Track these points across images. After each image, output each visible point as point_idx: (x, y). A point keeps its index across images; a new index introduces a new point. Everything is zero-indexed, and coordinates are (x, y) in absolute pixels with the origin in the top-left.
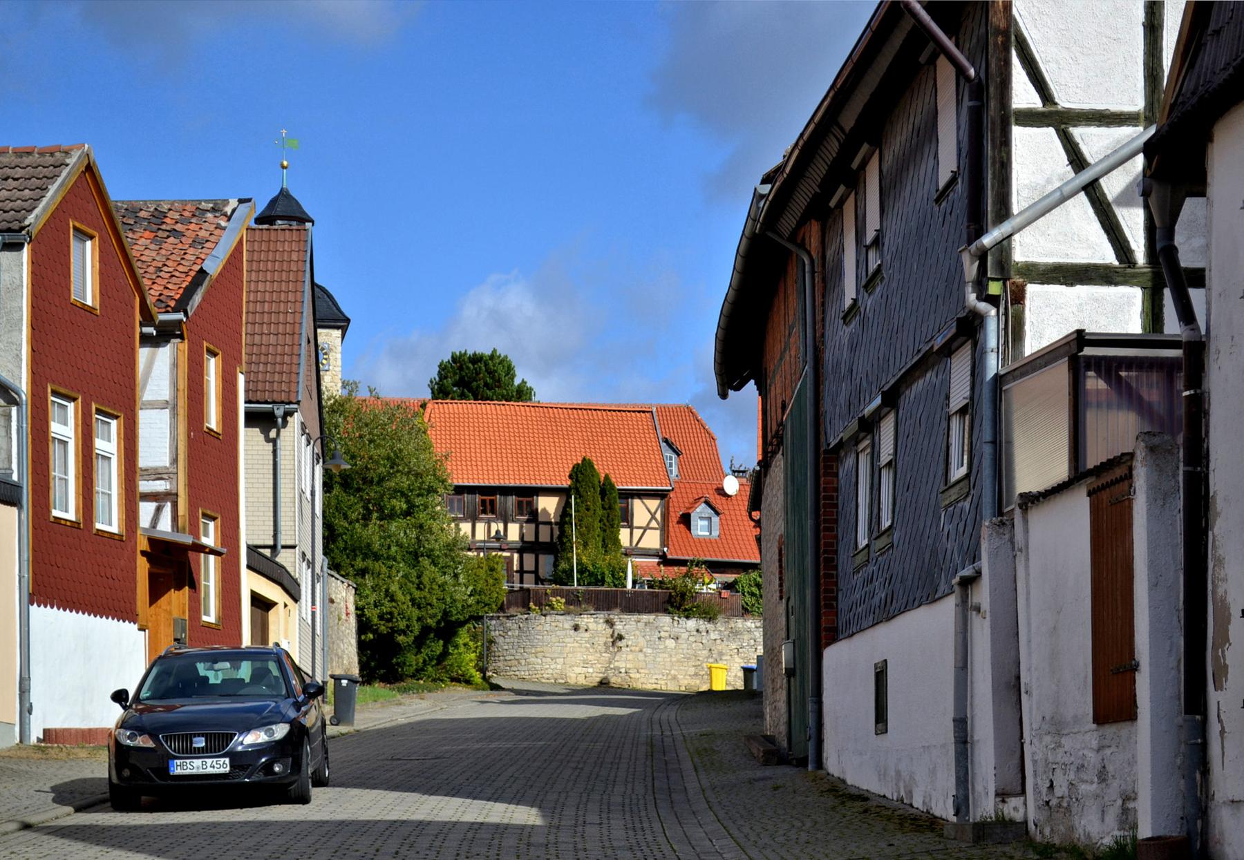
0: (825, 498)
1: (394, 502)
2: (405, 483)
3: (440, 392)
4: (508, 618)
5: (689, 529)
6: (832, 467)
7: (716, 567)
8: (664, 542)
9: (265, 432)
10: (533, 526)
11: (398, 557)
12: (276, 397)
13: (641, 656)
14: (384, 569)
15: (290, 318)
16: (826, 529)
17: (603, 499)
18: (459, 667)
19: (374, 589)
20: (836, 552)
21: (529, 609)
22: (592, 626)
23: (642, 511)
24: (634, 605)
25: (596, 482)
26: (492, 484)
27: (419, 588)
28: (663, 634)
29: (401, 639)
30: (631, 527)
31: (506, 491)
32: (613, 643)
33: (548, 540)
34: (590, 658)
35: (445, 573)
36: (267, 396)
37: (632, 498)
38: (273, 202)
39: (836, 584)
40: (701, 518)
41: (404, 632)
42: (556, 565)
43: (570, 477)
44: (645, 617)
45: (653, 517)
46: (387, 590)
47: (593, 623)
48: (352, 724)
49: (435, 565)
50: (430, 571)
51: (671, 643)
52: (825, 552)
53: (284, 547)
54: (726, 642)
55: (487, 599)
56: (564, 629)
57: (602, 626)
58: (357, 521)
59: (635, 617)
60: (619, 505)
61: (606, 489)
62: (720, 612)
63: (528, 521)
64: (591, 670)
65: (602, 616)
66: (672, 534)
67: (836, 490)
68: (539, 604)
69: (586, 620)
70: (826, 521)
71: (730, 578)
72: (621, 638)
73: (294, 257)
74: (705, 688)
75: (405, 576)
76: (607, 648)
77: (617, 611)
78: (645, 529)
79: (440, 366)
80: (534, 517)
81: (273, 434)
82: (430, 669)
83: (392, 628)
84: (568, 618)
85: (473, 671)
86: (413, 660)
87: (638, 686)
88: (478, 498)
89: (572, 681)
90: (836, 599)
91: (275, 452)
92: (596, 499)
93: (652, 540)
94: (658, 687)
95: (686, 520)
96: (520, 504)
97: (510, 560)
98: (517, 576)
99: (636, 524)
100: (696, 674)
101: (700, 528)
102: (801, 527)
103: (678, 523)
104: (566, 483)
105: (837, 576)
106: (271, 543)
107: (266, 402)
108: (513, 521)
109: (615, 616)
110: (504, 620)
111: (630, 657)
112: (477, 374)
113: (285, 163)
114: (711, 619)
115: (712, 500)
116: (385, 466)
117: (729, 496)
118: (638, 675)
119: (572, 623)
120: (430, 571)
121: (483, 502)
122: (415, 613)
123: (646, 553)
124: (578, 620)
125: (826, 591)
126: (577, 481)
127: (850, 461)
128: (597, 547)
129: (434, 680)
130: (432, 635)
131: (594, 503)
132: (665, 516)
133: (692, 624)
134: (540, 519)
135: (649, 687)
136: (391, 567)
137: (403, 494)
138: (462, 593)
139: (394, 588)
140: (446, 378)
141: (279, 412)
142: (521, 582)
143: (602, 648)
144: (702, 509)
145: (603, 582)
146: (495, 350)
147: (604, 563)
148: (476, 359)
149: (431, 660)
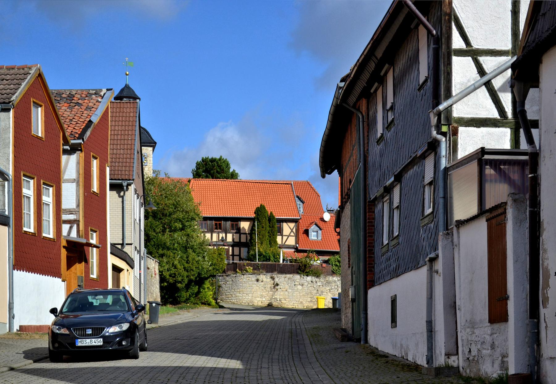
0: (369, 222)
1: (176, 224)
2: (181, 216)
3: (197, 175)
4: (227, 276)
5: (308, 236)
6: (372, 209)
7: (320, 253)
8: (297, 242)
9: (119, 193)
10: (238, 235)
11: (178, 249)
12: (123, 177)
13: (286, 293)
14: (172, 254)
15: (129, 142)
16: (369, 236)
17: (269, 223)
18: (205, 298)
19: (167, 263)
20: (374, 247)
21: (237, 272)
22: (265, 280)
23: (287, 228)
24: (283, 270)
25: (266, 215)
26: (220, 216)
27: (187, 263)
28: (296, 283)
29: (179, 285)
30: (282, 235)
31: (226, 219)
32: (274, 287)
33: (245, 241)
34: (264, 294)
35: (199, 256)
36: (119, 177)
37: (283, 222)
38: (122, 90)
39: (374, 261)
40: (313, 231)
41: (180, 282)
42: (248, 252)
43: (255, 213)
44: (288, 276)
45: (292, 231)
46: (173, 264)
47: (265, 278)
48: (157, 323)
49: (195, 252)
50: (192, 255)
51: (300, 287)
52: (369, 246)
53: (127, 244)
54: (324, 287)
55: (217, 268)
56: (252, 281)
57: (269, 280)
58: (160, 232)
59: (284, 275)
60: (277, 225)
61: (271, 218)
62: (322, 273)
63: (236, 233)
64: (264, 299)
65: (269, 275)
66: (300, 238)
67: (374, 219)
68: (241, 270)
69: (262, 277)
70: (369, 233)
71: (326, 258)
72: (277, 285)
73: (132, 115)
74: (315, 307)
75: (181, 257)
76: (271, 289)
77: (276, 273)
78: (288, 236)
79: (197, 163)
80: (238, 231)
81: (122, 194)
82: (192, 299)
83: (175, 280)
84: (254, 276)
85: (211, 300)
86: (185, 295)
87: (285, 306)
88: (214, 222)
89: (256, 304)
90: (374, 267)
91: (123, 202)
92: (266, 223)
93: (291, 241)
94: (294, 307)
95: (306, 232)
96: (232, 225)
97: (228, 250)
98: (231, 257)
99: (284, 234)
100: (311, 301)
101: (313, 236)
102: (358, 235)
103: (303, 233)
104: (253, 216)
105: (374, 257)
106: (121, 242)
107: (119, 180)
108: (229, 233)
109: (275, 275)
110: (225, 277)
111: (282, 293)
112: (213, 167)
113: (127, 73)
114: (318, 277)
115: (318, 223)
116: (172, 208)
117: (326, 222)
118: (285, 302)
119: (256, 278)
120: (192, 255)
121: (216, 224)
122: (186, 274)
123: (289, 247)
124: (258, 277)
125: (369, 264)
126: (258, 215)
127: (380, 206)
128: (267, 244)
129: (194, 304)
130: (193, 284)
131: (266, 225)
132: (297, 230)
133: (309, 278)
134: (242, 232)
135: (290, 307)
136: (175, 253)
137: (180, 221)
138: (207, 265)
139: (176, 262)
140: (199, 169)
141: (125, 184)
142: (233, 260)
143: (269, 289)
144: (314, 227)
145: (269, 260)
146: (221, 156)
147: (270, 251)
148: (213, 160)
149: (193, 295)
